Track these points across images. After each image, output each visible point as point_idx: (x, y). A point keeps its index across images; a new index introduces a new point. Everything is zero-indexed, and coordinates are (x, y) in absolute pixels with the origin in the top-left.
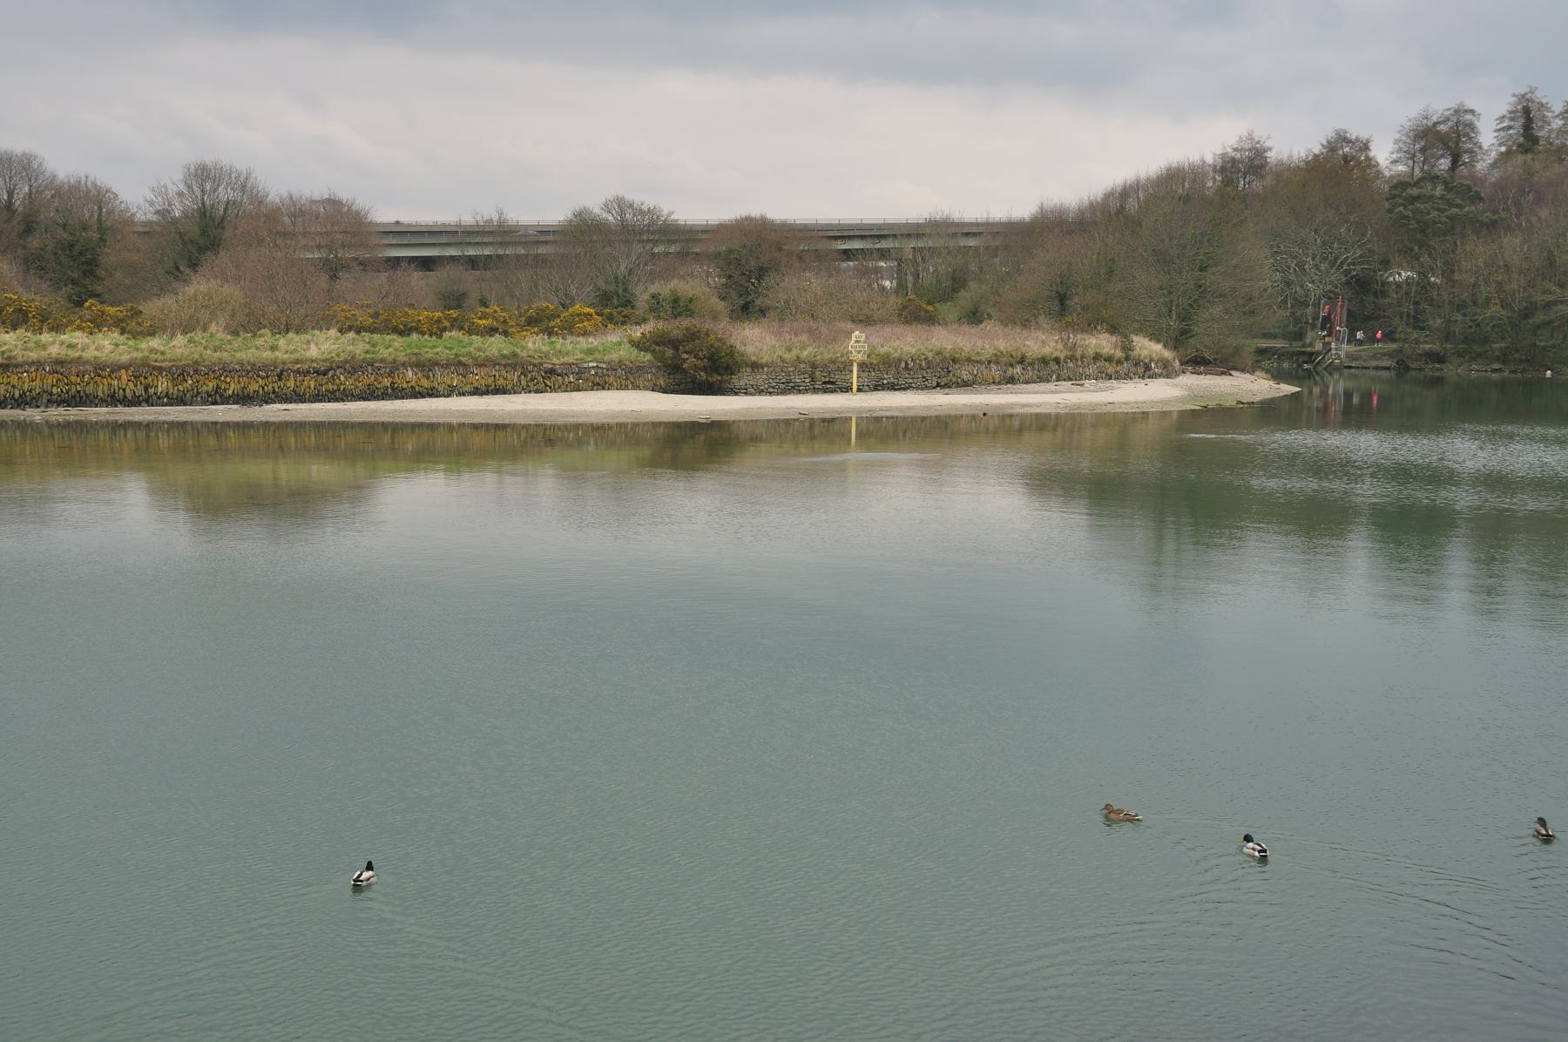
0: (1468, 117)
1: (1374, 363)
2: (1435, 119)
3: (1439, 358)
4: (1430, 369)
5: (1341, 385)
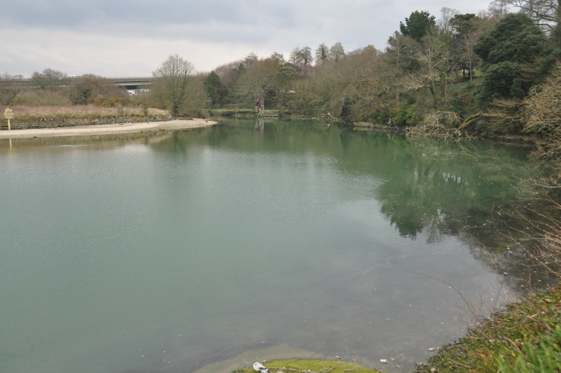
0: (309, 50)
1: (273, 115)
2: (300, 50)
3: (289, 114)
4: (288, 117)
5: (263, 121)
